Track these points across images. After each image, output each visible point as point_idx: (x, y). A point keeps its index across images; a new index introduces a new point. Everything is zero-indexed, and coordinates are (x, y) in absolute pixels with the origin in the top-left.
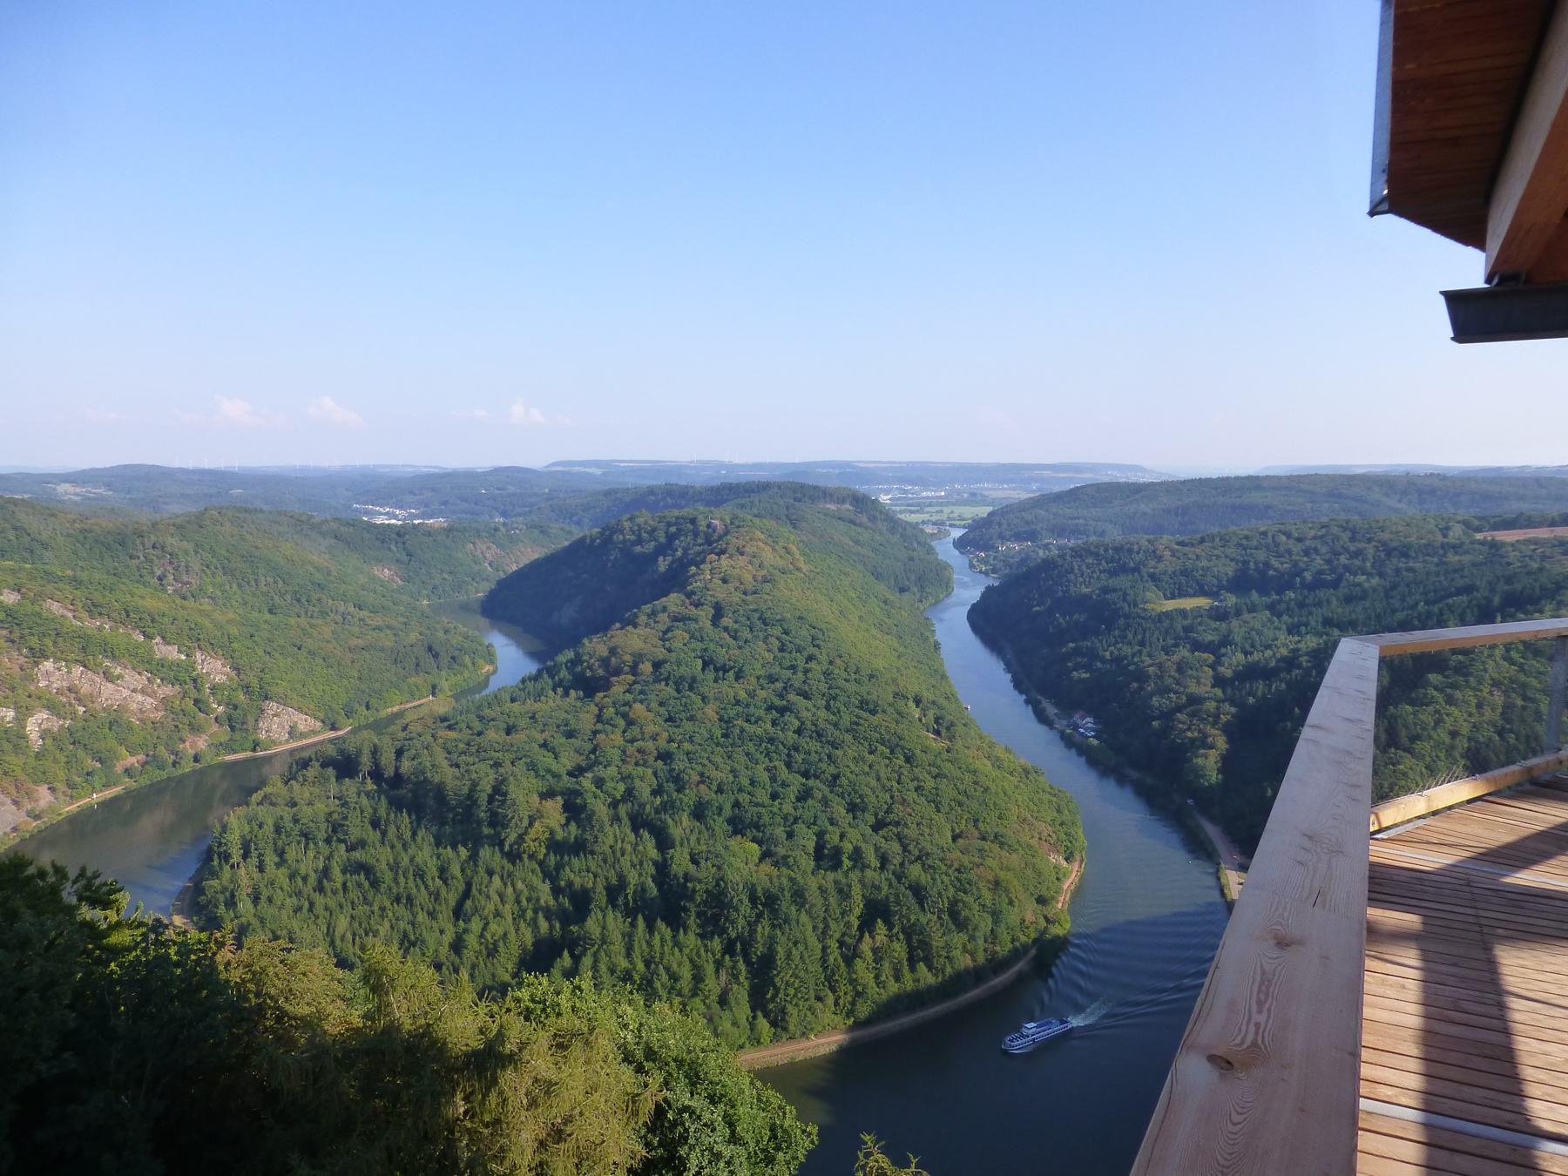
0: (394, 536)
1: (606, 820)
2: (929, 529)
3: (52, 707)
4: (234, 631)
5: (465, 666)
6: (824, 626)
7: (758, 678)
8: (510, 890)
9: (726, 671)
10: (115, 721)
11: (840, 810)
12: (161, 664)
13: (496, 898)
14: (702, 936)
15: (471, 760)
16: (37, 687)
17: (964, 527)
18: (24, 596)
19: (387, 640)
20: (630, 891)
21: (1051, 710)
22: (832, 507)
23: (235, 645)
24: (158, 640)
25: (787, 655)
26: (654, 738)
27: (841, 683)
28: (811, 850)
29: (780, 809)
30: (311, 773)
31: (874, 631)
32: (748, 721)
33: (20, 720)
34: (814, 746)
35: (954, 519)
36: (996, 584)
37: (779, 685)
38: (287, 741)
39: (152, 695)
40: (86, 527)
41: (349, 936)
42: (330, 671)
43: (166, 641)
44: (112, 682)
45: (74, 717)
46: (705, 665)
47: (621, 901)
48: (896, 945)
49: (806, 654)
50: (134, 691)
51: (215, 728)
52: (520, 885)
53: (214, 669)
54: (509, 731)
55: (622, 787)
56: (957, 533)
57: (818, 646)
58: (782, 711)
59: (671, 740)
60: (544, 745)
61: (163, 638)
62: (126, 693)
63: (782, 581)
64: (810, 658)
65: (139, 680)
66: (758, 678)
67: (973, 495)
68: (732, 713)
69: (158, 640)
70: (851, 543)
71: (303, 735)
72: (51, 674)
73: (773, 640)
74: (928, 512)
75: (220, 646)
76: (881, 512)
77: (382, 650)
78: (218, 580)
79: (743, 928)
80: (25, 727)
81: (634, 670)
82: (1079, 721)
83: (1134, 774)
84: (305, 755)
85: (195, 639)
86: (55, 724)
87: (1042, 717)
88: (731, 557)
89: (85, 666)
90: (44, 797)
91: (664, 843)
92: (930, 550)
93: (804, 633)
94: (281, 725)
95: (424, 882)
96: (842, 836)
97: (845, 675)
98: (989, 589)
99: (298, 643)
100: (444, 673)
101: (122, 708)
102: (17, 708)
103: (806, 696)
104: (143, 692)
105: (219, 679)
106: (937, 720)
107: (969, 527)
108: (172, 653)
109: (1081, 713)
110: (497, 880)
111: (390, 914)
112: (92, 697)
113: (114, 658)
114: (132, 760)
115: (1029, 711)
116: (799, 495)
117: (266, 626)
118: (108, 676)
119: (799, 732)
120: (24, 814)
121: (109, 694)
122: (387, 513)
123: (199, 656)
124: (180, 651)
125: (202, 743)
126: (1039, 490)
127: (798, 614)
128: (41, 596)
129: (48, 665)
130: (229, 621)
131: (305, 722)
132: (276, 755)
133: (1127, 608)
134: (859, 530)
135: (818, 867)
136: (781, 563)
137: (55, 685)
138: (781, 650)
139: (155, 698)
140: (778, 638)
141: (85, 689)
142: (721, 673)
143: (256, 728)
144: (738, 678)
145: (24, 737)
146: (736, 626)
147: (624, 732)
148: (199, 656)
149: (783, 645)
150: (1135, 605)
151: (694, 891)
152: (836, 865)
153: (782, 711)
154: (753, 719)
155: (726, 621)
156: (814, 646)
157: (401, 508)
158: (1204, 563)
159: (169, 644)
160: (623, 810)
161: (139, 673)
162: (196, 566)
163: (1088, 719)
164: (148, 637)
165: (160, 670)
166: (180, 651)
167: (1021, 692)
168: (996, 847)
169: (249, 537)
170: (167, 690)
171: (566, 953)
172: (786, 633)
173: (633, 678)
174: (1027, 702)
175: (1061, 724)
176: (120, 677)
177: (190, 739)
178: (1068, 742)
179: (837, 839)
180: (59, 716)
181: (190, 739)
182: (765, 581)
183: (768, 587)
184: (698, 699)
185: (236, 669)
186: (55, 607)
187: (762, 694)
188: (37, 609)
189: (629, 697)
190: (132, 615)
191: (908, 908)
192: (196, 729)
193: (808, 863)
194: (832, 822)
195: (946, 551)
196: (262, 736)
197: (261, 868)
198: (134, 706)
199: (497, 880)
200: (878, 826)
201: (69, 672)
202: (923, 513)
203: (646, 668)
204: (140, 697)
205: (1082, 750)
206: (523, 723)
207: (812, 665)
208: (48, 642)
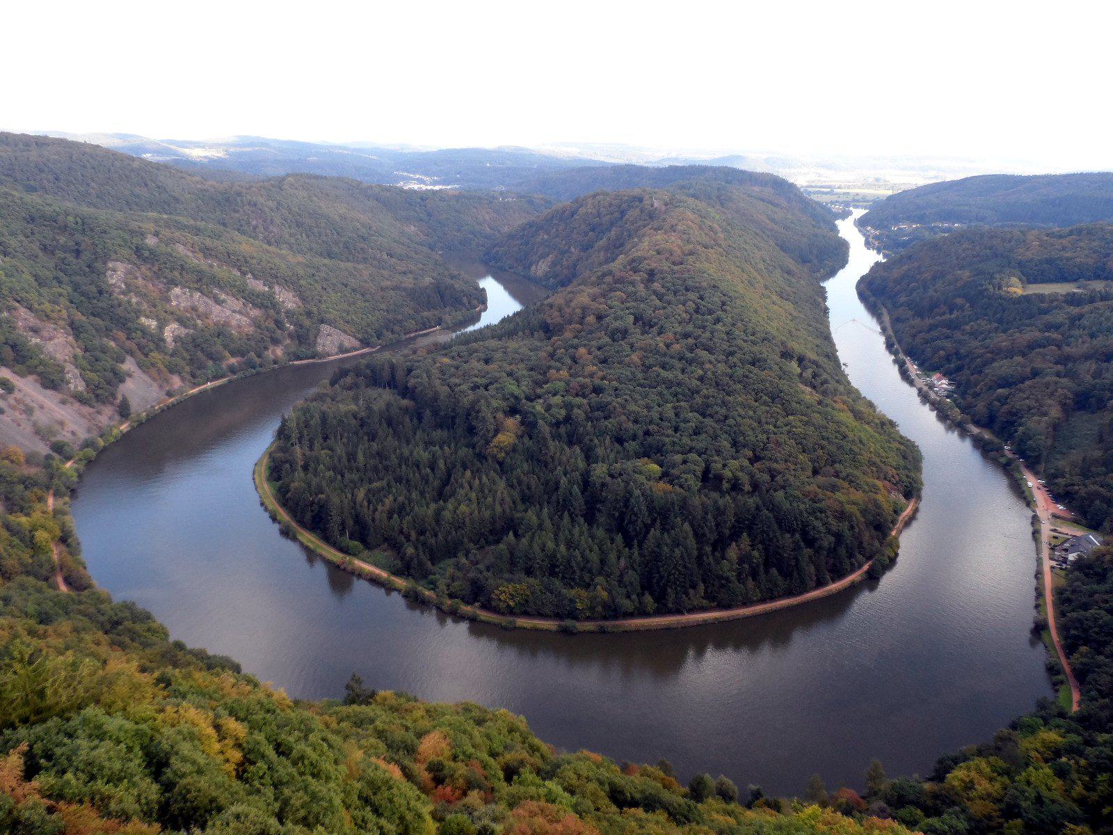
0: (419, 200)
1: (548, 436)
2: (837, 208)
3: (182, 321)
4: (301, 272)
5: (464, 305)
6: (732, 294)
7: (675, 333)
8: (477, 481)
9: (651, 326)
10: (221, 332)
11: (725, 444)
12: (252, 293)
13: (466, 485)
14: (609, 531)
15: (457, 381)
16: (171, 305)
17: (865, 208)
18: (161, 240)
19: (408, 282)
20: (561, 491)
21: (913, 368)
22: (756, 189)
23: (302, 282)
24: (249, 276)
25: (700, 317)
26: (592, 375)
27: (740, 342)
28: (699, 474)
29: (680, 440)
30: (349, 380)
31: (774, 297)
32: (663, 368)
33: (161, 328)
34: (712, 391)
35: (858, 201)
36: (884, 261)
37: (691, 341)
38: (337, 354)
39: (247, 315)
40: (205, 187)
41: (365, 503)
42: (367, 304)
43: (255, 277)
44: (219, 304)
45: (195, 327)
46: (636, 320)
47: (554, 498)
48: (755, 553)
49: (715, 316)
50: (234, 311)
51: (288, 341)
52: (484, 478)
53: (287, 299)
54: (487, 361)
55: (563, 412)
56: (858, 213)
57: (725, 311)
58: (690, 362)
59: (603, 378)
60: (510, 374)
61: (253, 274)
62: (228, 313)
63: (703, 255)
64: (718, 320)
65: (237, 304)
66: (675, 333)
67: (877, 180)
68: (651, 361)
69: (249, 276)
70: (768, 222)
71: (347, 351)
72: (180, 297)
73: (690, 303)
74: (836, 194)
75: (291, 283)
76: (795, 195)
77: (405, 289)
78: (293, 231)
79: (640, 529)
80: (163, 334)
81: (582, 320)
82: (936, 382)
83: (975, 430)
84: (347, 366)
85: (273, 277)
86: (183, 332)
87: (905, 375)
88: (666, 233)
89: (201, 292)
90: (176, 382)
91: (589, 456)
92: (834, 229)
93: (716, 299)
94: (332, 342)
95: (418, 469)
96: (724, 466)
97: (743, 336)
98: (877, 264)
99: (345, 282)
100: (448, 309)
101: (226, 324)
102: (158, 320)
103: (709, 350)
104: (240, 313)
105: (290, 305)
106: (815, 376)
107: (870, 208)
108: (259, 286)
109: (938, 375)
110: (468, 473)
111: (394, 491)
112: (206, 316)
113: (221, 288)
114: (233, 361)
115: (895, 370)
116: (730, 178)
117: (324, 268)
118: (219, 302)
119: (701, 379)
120: (164, 393)
121: (218, 314)
122: (418, 179)
123: (277, 289)
124: (265, 285)
125: (279, 352)
126: (935, 177)
127: (713, 283)
128: (173, 241)
129: (177, 290)
130: (299, 263)
131: (349, 341)
132: (328, 362)
133: (992, 290)
134: (776, 209)
135: (704, 487)
136: (706, 240)
137: (182, 305)
138: (697, 311)
139: (248, 317)
140: (694, 302)
141: (202, 309)
142: (647, 328)
143: (315, 342)
144: (659, 334)
145: (163, 340)
146: (663, 291)
147: (570, 368)
148: (277, 289)
149: (698, 308)
150: (1000, 288)
151: (606, 498)
152: (717, 488)
153: (690, 362)
154: (668, 366)
155: (656, 286)
156: (722, 310)
157: (427, 175)
158: (1069, 254)
159: (257, 279)
160: (563, 430)
161: (237, 299)
162: (278, 221)
163: (944, 381)
164: (244, 274)
165: (252, 298)
166: (265, 285)
167: (891, 352)
168: (846, 485)
169: (315, 199)
170: (255, 313)
171: (511, 533)
172: (701, 298)
173: (581, 327)
174: (895, 361)
175: (920, 382)
176: (224, 301)
177: (271, 348)
178: (924, 397)
179: (719, 466)
180: (186, 327)
181: (271, 348)
182: (691, 253)
183: (691, 259)
184: (628, 348)
185: (303, 299)
186: (180, 248)
187: (676, 347)
188: (169, 250)
189: (576, 341)
190: (232, 257)
191: (769, 527)
192: (275, 341)
193: (695, 484)
194: (718, 452)
195: (847, 230)
196: (320, 349)
197: (311, 448)
198: (234, 323)
199: (468, 473)
200: (755, 459)
201: (191, 296)
202: (833, 194)
203: (591, 319)
204: (238, 316)
205: (936, 406)
206: (498, 355)
207: (719, 326)
208: (176, 273)
